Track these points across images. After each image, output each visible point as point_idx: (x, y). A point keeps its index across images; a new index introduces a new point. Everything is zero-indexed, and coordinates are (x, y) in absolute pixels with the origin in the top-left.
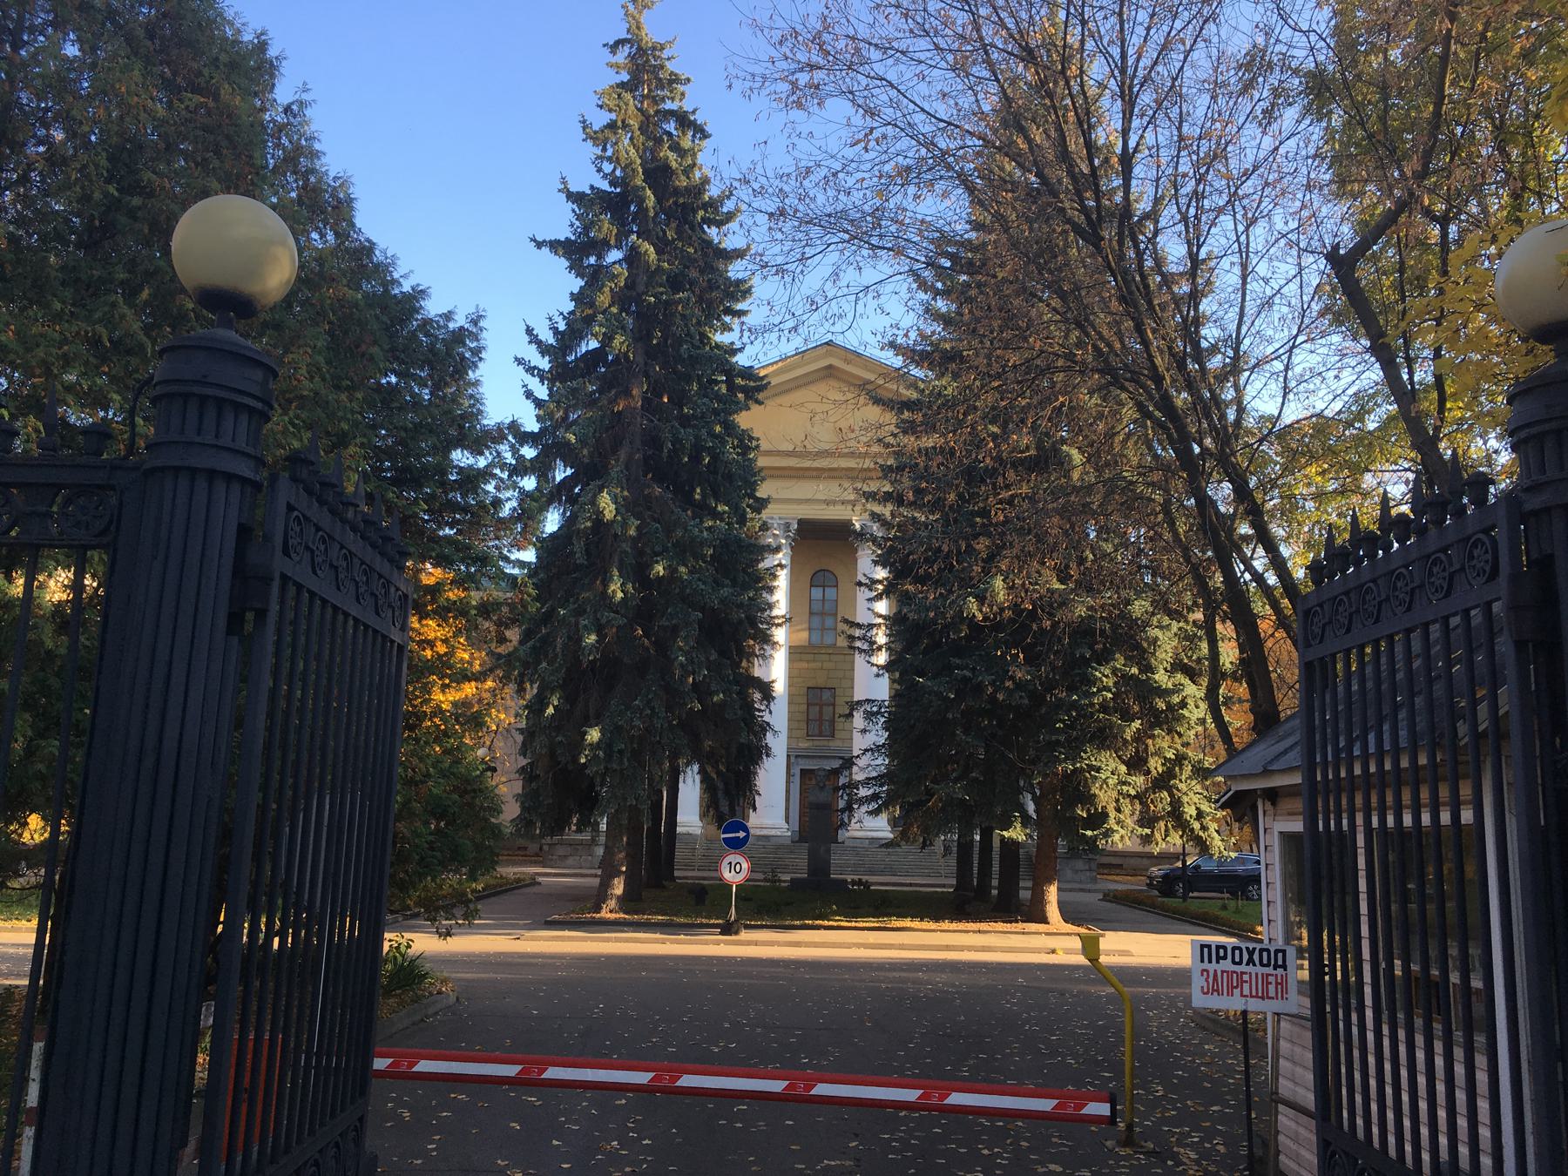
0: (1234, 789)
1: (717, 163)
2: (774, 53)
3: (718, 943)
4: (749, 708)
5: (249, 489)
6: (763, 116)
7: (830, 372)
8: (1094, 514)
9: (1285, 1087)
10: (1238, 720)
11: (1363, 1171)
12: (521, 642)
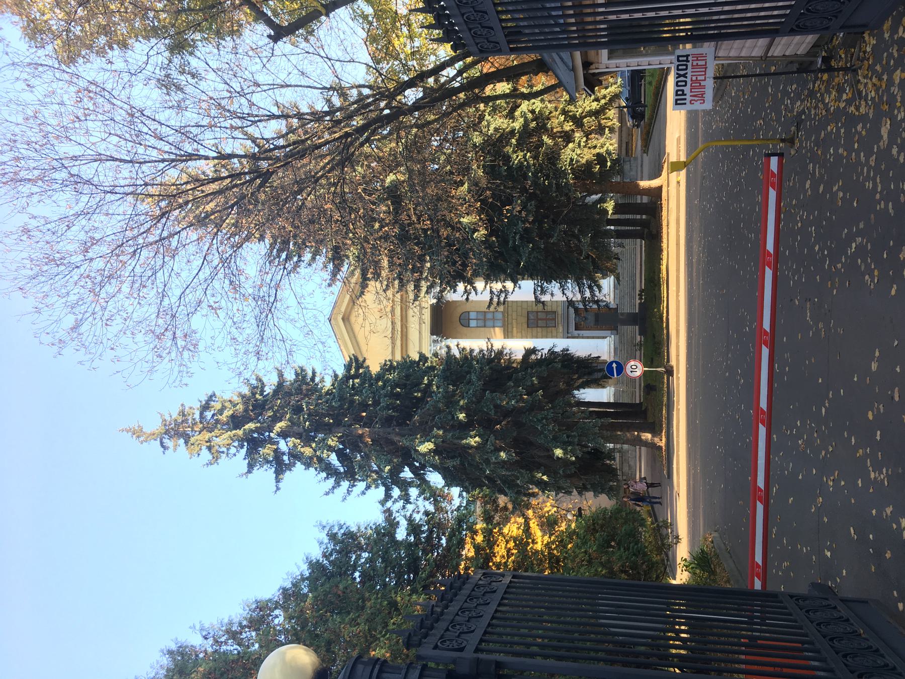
0: (583, 86)
1: (231, 389)
2: (167, 359)
3: (678, 378)
5: (427, 673)
6: (202, 365)
7: (346, 319)
8: (424, 167)
9: (757, 52)
10: (542, 81)
11: (808, 10)
12: (506, 495)
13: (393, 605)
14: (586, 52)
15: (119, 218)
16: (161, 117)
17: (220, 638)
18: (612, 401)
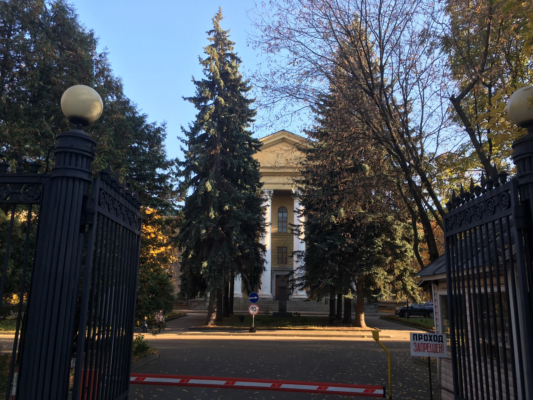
1: (244, 71)
3: (248, 335)
6: (260, 55)
7: (283, 140)
8: (374, 187)
9: (444, 383)
10: (425, 256)
12: (180, 233)
13: (119, 166)
15: (347, 8)
17: (100, 64)
18: (234, 296)
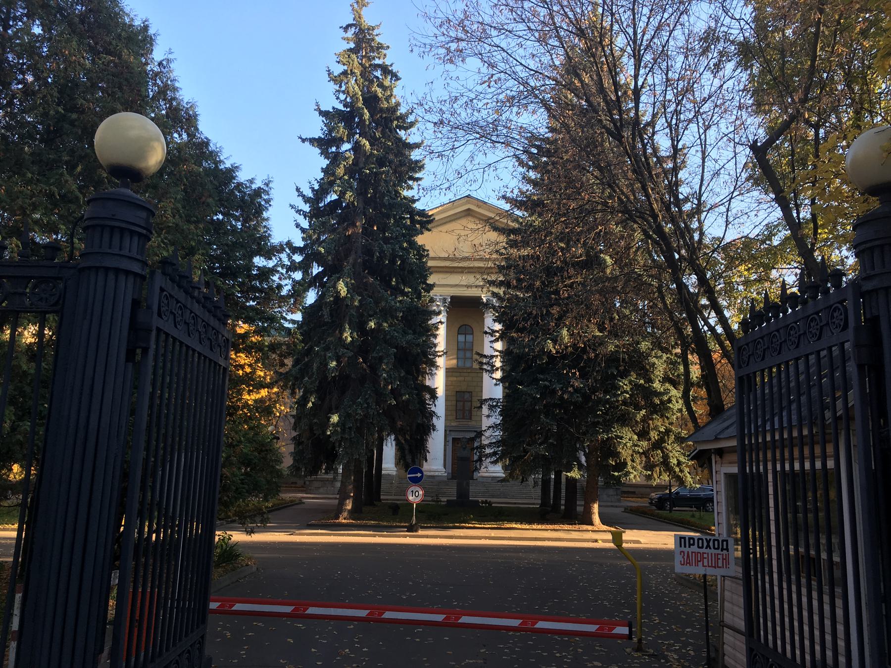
1: (404, 94)
3: (405, 536)
4: (423, 403)
6: (431, 67)
7: (468, 213)
8: (619, 293)
10: (701, 410)
12: (293, 366)
13: (191, 252)
14: (735, 452)
16: (677, 33)
17: (160, 78)
